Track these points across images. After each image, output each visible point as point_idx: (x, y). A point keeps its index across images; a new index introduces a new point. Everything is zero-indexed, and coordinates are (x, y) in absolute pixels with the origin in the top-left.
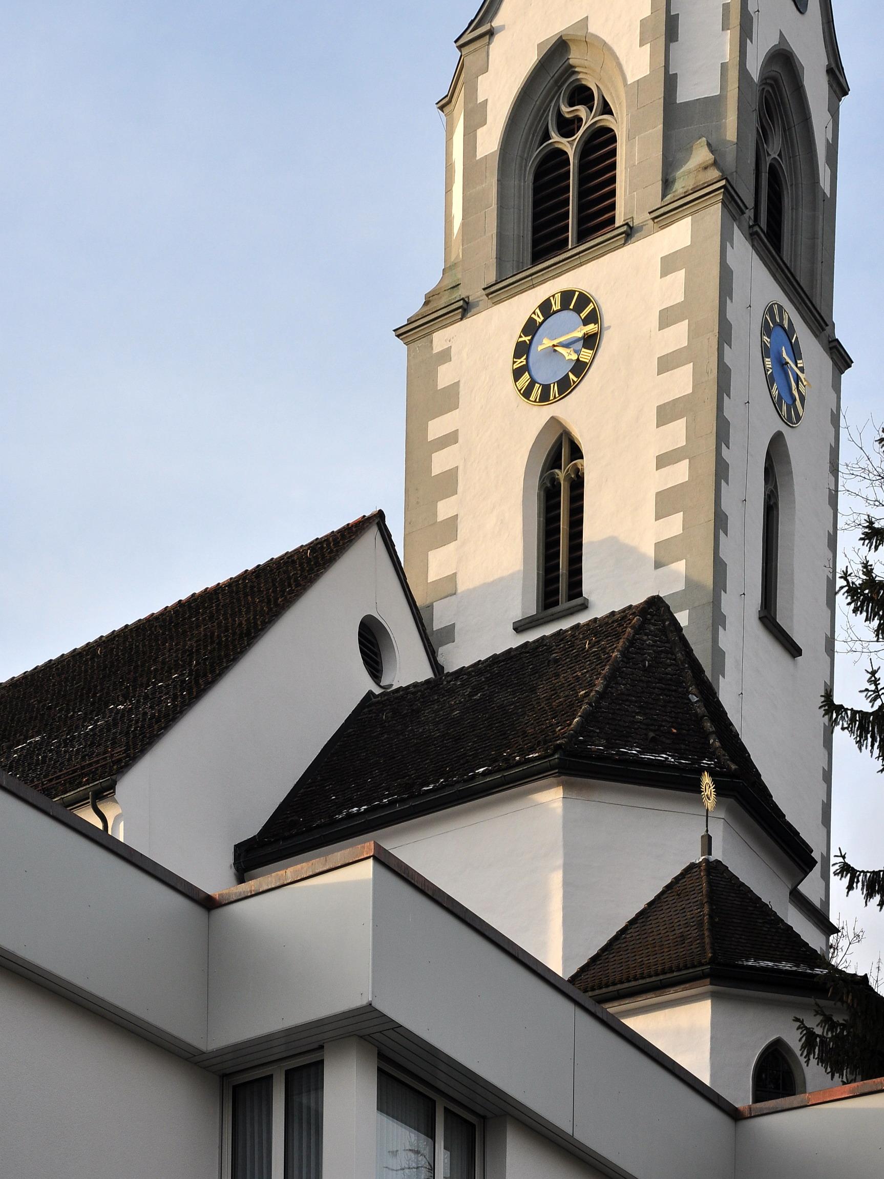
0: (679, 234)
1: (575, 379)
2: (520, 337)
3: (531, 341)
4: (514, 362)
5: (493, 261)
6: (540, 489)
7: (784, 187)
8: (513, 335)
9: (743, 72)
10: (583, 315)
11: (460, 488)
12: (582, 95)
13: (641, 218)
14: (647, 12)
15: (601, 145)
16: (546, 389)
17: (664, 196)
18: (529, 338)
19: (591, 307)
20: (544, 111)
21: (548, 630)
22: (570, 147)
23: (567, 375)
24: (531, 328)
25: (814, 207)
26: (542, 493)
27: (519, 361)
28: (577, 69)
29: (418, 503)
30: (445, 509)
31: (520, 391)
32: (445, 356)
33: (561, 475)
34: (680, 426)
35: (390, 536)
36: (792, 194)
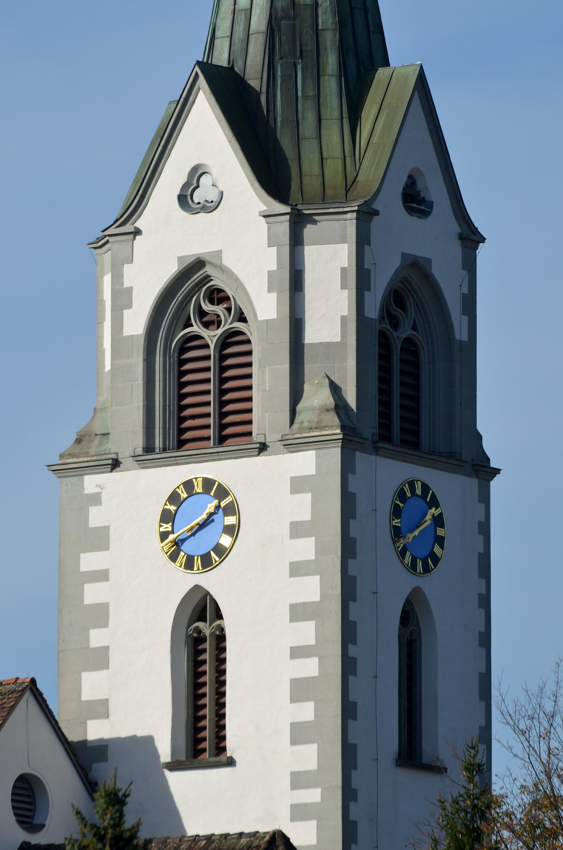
0: (305, 462)
1: (217, 559)
2: (166, 504)
3: (176, 511)
4: (160, 526)
8: (158, 504)
12: (218, 296)
13: (271, 438)
14: (274, 267)
17: (292, 423)
21: (331, 61)
23: (209, 552)
24: (174, 498)
27: (165, 525)
28: (211, 278)
30: (97, 638)
31: (167, 553)
32: (96, 499)
35: (41, 694)
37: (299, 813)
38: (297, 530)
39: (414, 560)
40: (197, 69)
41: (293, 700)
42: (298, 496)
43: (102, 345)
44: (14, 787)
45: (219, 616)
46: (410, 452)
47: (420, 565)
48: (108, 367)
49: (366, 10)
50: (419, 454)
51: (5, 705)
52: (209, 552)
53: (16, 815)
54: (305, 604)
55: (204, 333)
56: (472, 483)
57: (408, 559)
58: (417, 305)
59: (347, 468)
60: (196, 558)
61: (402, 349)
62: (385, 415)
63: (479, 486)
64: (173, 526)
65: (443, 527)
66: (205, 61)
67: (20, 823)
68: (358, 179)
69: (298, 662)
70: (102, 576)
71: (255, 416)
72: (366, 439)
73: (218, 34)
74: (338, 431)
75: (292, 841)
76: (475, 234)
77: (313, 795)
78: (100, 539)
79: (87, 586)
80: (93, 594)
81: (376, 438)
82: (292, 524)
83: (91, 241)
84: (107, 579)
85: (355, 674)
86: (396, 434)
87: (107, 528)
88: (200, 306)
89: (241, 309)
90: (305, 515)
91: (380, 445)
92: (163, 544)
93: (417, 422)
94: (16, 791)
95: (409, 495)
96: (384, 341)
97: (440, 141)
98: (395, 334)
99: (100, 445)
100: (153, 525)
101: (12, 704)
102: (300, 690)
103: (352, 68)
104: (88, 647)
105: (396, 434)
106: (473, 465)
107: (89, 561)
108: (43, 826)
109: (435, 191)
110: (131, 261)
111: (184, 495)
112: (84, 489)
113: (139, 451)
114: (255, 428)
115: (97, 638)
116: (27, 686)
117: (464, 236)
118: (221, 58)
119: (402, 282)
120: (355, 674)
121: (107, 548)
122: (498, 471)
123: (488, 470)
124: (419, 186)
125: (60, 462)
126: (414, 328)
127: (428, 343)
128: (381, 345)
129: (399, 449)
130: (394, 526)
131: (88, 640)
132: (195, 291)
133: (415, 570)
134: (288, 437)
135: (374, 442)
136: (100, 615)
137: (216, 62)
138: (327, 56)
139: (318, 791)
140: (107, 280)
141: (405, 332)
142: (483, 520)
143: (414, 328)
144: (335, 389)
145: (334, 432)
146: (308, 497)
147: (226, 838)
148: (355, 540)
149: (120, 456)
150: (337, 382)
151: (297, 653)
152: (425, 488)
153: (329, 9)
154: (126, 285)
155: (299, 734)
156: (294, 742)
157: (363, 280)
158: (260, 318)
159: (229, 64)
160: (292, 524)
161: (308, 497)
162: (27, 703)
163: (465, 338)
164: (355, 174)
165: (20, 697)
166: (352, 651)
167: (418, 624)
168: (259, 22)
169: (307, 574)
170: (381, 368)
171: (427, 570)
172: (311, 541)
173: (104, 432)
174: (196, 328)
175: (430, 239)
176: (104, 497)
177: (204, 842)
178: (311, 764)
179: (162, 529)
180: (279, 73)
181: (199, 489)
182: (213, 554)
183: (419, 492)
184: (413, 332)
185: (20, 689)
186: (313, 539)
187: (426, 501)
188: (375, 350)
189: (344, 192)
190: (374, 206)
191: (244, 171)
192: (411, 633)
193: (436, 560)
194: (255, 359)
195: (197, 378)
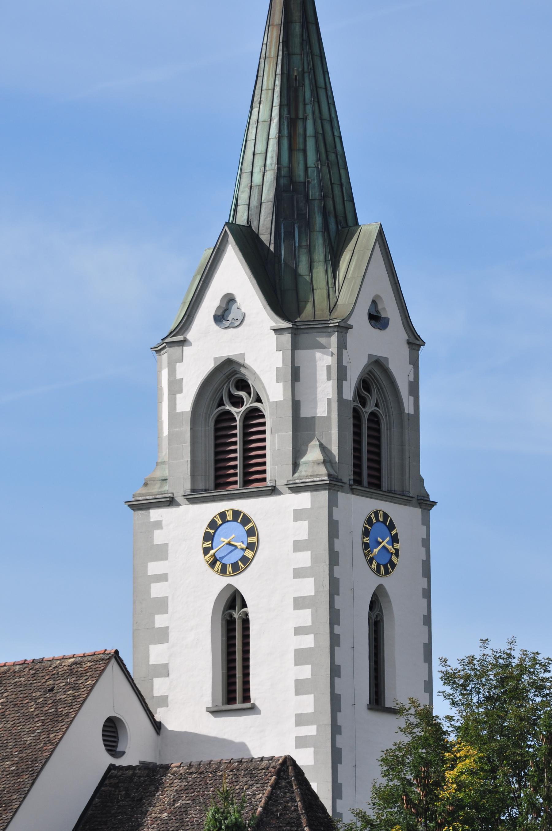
0: (304, 499)
1: (243, 566)
4: (203, 543)
5: (188, 477)
6: (222, 620)
7: (380, 417)
8: (202, 528)
9: (341, 400)
10: (247, 528)
11: (170, 610)
13: (281, 483)
14: (280, 365)
15: (254, 415)
16: (224, 567)
17: (294, 473)
18: (213, 531)
19: (250, 525)
20: (220, 389)
22: (238, 412)
24: (213, 525)
25: (401, 426)
26: (224, 622)
29: (142, 611)
30: (160, 621)
31: (208, 562)
32: (158, 525)
33: (236, 615)
34: (307, 613)
35: (122, 661)
36: (387, 421)
37: (301, 742)
38: (298, 546)
39: (378, 566)
40: (226, 228)
41: (296, 664)
42: (298, 523)
43: (161, 418)
44: (104, 726)
45: (244, 605)
46: (375, 491)
47: (382, 569)
48: (165, 432)
49: (341, 185)
50: (381, 493)
51: (98, 669)
52: (237, 562)
53: (105, 745)
54: (304, 598)
55: (233, 410)
56: (417, 512)
57: (374, 565)
58: (378, 389)
59: (332, 503)
60: (228, 565)
61: (369, 420)
62: (357, 466)
63: (422, 514)
64: (212, 543)
65: (398, 542)
66: (230, 222)
67: (108, 750)
68: (338, 303)
69: (299, 637)
70: (163, 578)
71: (268, 467)
72: (345, 483)
73: (239, 202)
74: (326, 478)
75: (297, 763)
76: (418, 340)
77: (311, 730)
78: (161, 553)
79: (152, 585)
80: (157, 590)
81: (352, 482)
82: (295, 542)
83: (153, 346)
84: (166, 580)
85: (339, 646)
86: (365, 479)
87: (167, 545)
88: (229, 391)
89: (258, 394)
90: (304, 536)
91: (355, 487)
92: (207, 557)
93: (379, 470)
94: (105, 729)
95: (374, 521)
96: (357, 415)
97: (385, 249)
98: (364, 410)
99: (160, 487)
100: (198, 543)
101: (102, 668)
102: (301, 656)
103: (332, 226)
104: (154, 628)
105: (365, 479)
106: (418, 500)
107: (154, 568)
108: (124, 753)
109: (390, 310)
110: (182, 361)
111: (220, 522)
112: (150, 518)
113: (188, 492)
114: (268, 476)
115: (160, 621)
116: (112, 655)
117: (411, 341)
118: (241, 219)
119: (368, 374)
120: (339, 646)
121: (166, 559)
122: (435, 503)
123: (428, 503)
124: (380, 307)
125: (134, 499)
126: (377, 405)
127: (386, 416)
128: (354, 417)
129: (368, 490)
130: (365, 543)
131: (153, 622)
132: (229, 381)
133: (380, 573)
134: (291, 482)
135: (350, 485)
136: (162, 605)
137: (238, 223)
138: (316, 218)
139: (315, 727)
140: (165, 373)
141: (370, 408)
142: (425, 537)
143: (377, 405)
144: (323, 449)
145: (323, 478)
146: (305, 523)
147: (251, 761)
148: (338, 553)
149: (175, 495)
150: (324, 443)
151: (299, 631)
152: (386, 516)
153: (316, 185)
154: (178, 377)
155: (301, 687)
156: (297, 693)
157: (342, 374)
158: (271, 400)
159: (248, 223)
160: (295, 542)
161: (305, 523)
162: (113, 665)
163: (412, 412)
164: (336, 300)
165: (108, 663)
166: (337, 630)
167: (381, 610)
168: (269, 194)
169: (305, 577)
170: (354, 433)
171: (387, 572)
172: (308, 553)
173: (164, 478)
174: (229, 407)
175: (388, 345)
176: (164, 523)
177: (236, 764)
178: (310, 709)
179: (204, 546)
180: (283, 230)
181: (230, 518)
182: (240, 563)
183: (381, 519)
184: (376, 408)
185: (108, 657)
186: (309, 552)
187: (386, 525)
188: (350, 422)
189: (328, 313)
190: (349, 322)
191: (259, 298)
192: (377, 616)
193: (393, 566)
194: (268, 428)
195: (227, 441)
